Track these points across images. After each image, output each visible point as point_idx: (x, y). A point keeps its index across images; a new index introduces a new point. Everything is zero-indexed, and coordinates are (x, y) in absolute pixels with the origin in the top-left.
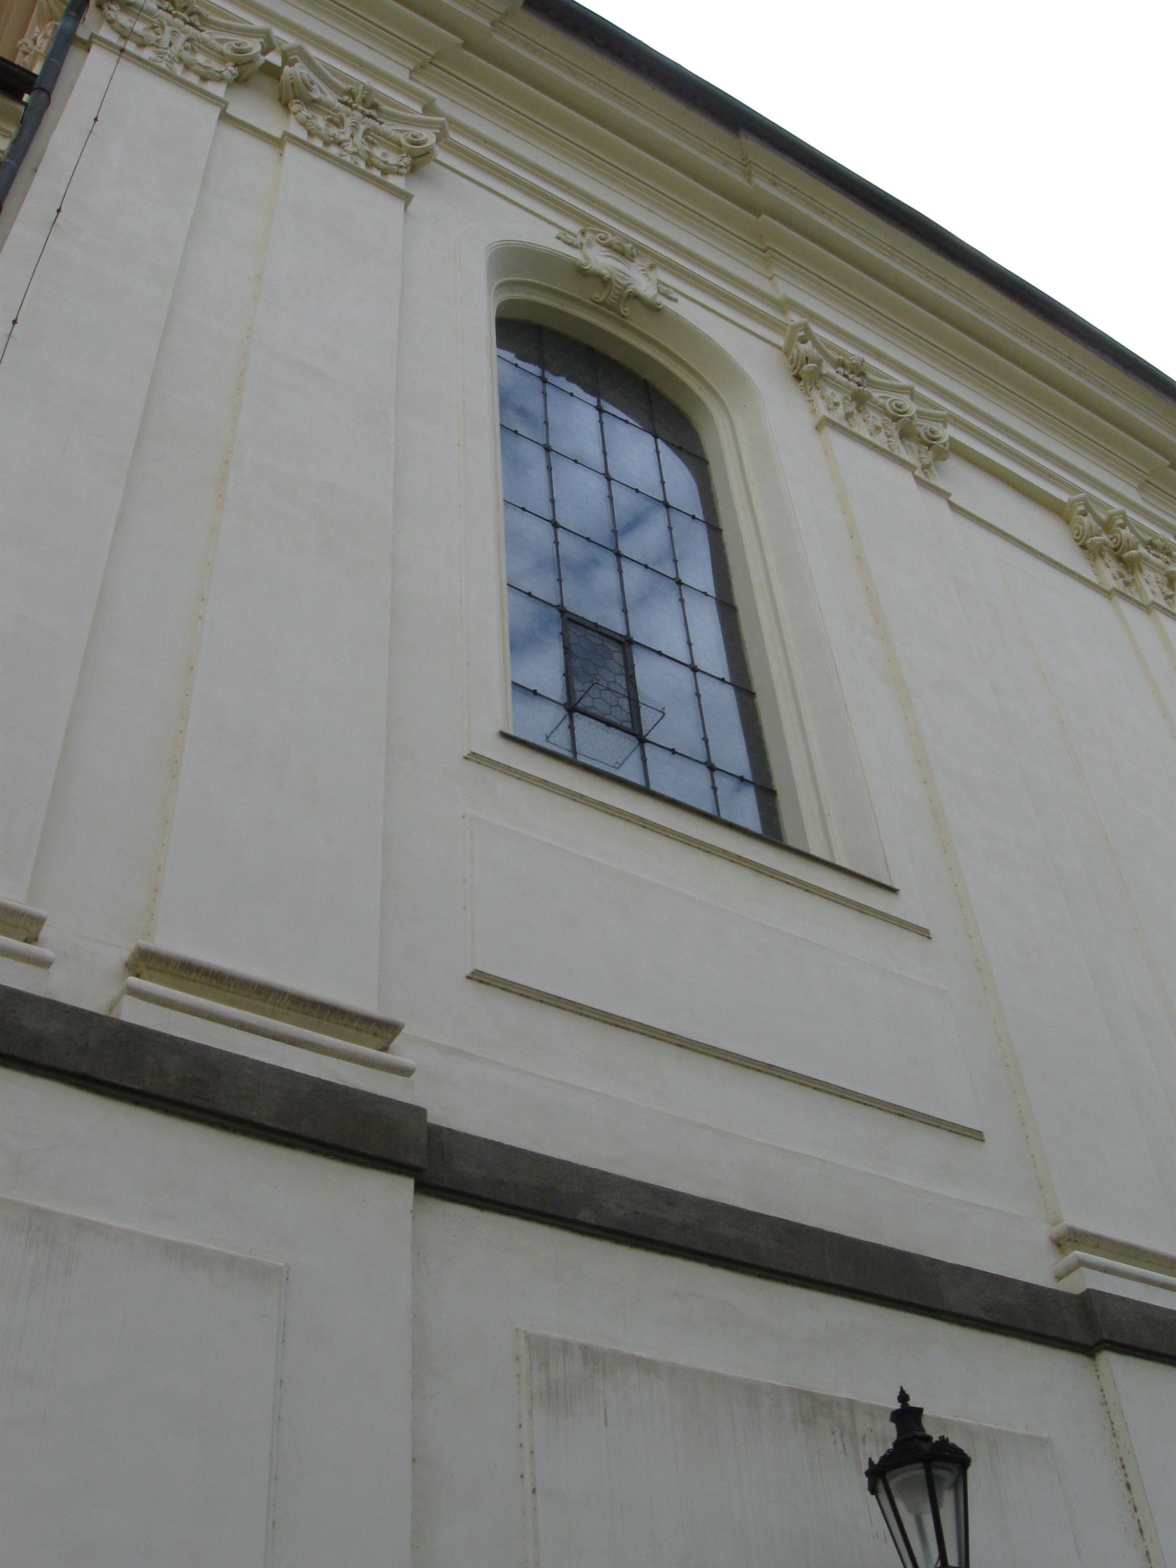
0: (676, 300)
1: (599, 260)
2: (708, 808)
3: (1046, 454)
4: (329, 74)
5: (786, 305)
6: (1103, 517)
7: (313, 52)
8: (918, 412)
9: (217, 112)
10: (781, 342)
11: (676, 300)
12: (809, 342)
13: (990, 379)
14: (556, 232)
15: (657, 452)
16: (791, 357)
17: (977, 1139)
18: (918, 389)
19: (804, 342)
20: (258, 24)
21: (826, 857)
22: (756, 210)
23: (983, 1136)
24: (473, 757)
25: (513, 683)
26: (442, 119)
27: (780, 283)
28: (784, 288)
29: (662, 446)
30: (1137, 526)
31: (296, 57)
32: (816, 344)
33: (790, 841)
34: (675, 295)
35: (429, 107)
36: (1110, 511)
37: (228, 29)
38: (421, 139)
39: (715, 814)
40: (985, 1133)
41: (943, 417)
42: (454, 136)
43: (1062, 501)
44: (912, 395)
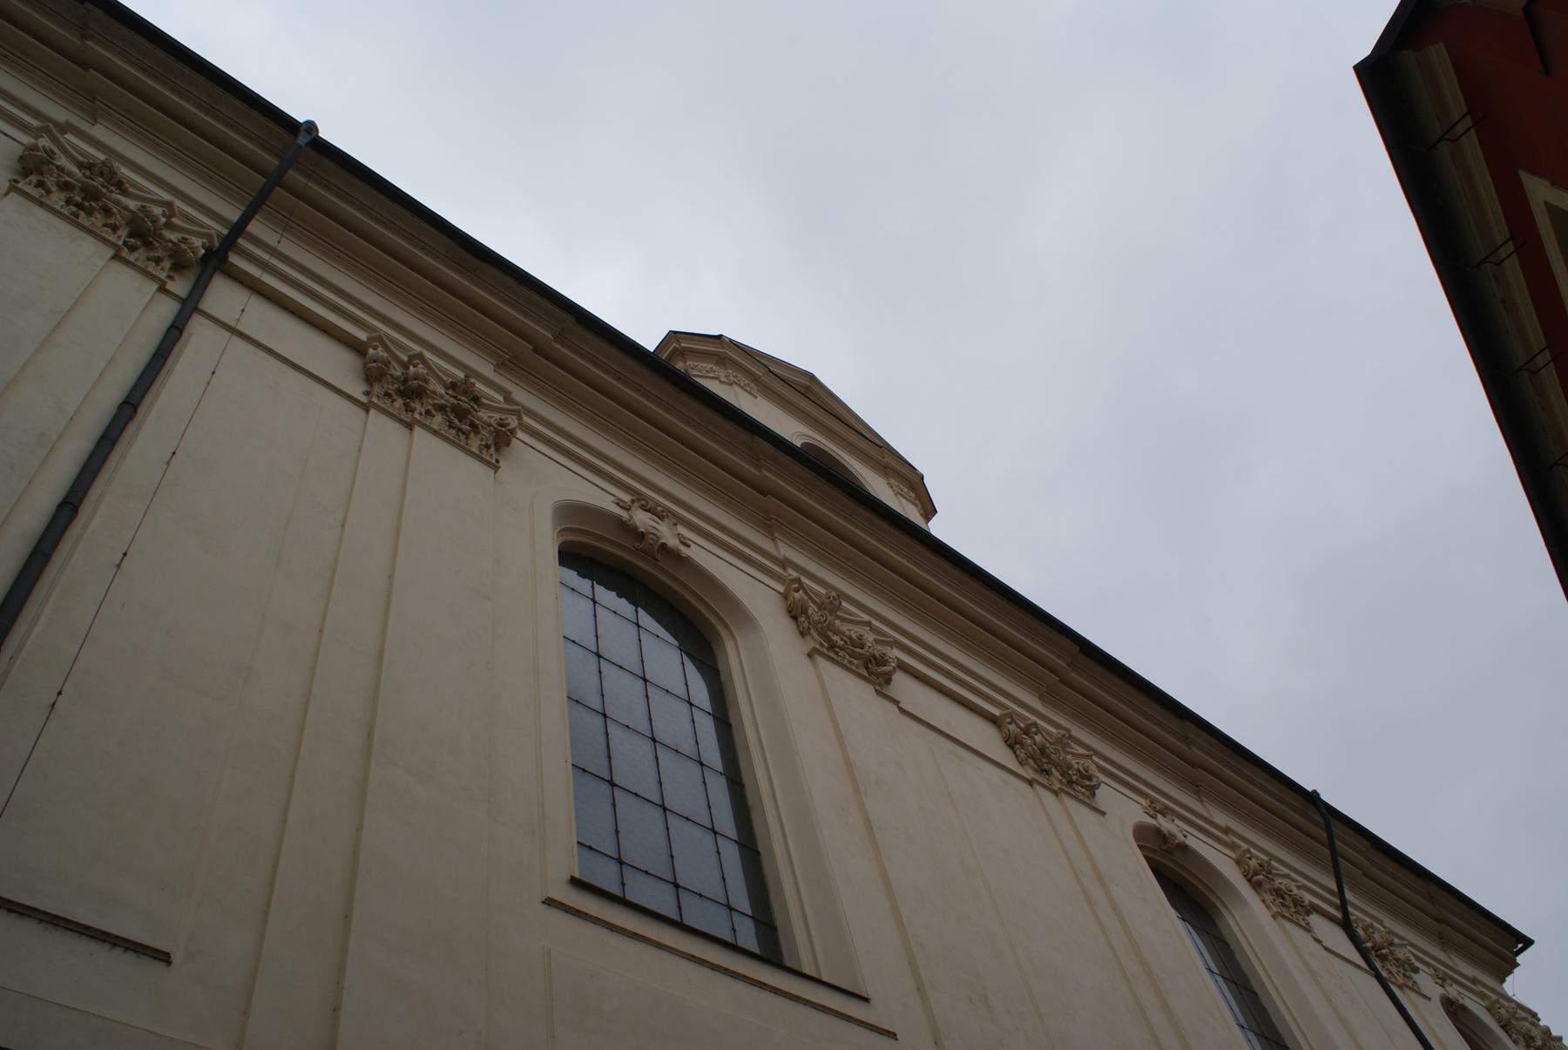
0: (689, 546)
1: (642, 519)
2: (674, 915)
3: (499, 388)
4: (67, 146)
5: (785, 563)
6: (1022, 725)
7: (428, 355)
8: (875, 640)
9: (155, 286)
10: (781, 589)
11: (689, 546)
12: (801, 591)
13: (247, 193)
14: (613, 498)
15: (683, 663)
16: (789, 603)
17: (164, 961)
18: (874, 622)
19: (797, 591)
20: (167, 197)
21: (814, 974)
22: (764, 492)
23: (169, 957)
24: (549, 902)
25: (578, 842)
26: (520, 408)
27: (780, 544)
28: (786, 551)
29: (683, 655)
30: (814, 593)
31: (418, 361)
32: (805, 592)
33: (788, 963)
34: (688, 542)
35: (508, 397)
36: (410, 353)
37: (852, 622)
38: (505, 422)
39: (621, 895)
40: (172, 955)
41: (891, 642)
42: (526, 419)
43: (994, 715)
44: (873, 629)
